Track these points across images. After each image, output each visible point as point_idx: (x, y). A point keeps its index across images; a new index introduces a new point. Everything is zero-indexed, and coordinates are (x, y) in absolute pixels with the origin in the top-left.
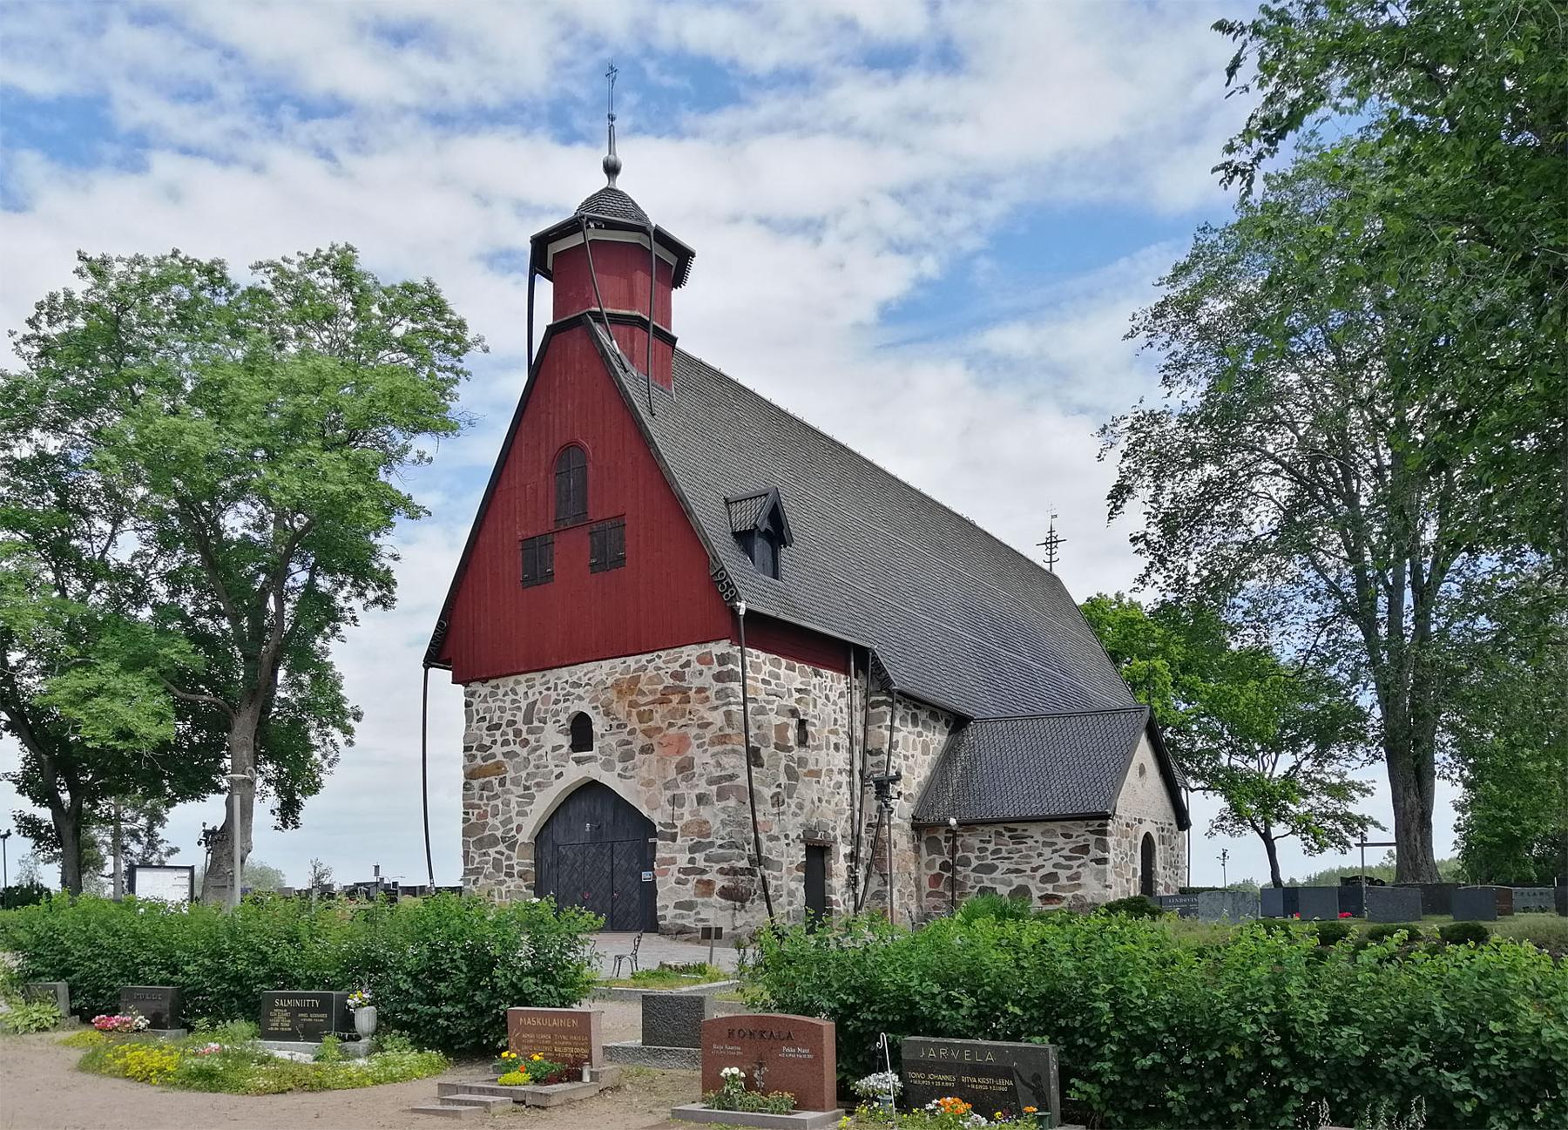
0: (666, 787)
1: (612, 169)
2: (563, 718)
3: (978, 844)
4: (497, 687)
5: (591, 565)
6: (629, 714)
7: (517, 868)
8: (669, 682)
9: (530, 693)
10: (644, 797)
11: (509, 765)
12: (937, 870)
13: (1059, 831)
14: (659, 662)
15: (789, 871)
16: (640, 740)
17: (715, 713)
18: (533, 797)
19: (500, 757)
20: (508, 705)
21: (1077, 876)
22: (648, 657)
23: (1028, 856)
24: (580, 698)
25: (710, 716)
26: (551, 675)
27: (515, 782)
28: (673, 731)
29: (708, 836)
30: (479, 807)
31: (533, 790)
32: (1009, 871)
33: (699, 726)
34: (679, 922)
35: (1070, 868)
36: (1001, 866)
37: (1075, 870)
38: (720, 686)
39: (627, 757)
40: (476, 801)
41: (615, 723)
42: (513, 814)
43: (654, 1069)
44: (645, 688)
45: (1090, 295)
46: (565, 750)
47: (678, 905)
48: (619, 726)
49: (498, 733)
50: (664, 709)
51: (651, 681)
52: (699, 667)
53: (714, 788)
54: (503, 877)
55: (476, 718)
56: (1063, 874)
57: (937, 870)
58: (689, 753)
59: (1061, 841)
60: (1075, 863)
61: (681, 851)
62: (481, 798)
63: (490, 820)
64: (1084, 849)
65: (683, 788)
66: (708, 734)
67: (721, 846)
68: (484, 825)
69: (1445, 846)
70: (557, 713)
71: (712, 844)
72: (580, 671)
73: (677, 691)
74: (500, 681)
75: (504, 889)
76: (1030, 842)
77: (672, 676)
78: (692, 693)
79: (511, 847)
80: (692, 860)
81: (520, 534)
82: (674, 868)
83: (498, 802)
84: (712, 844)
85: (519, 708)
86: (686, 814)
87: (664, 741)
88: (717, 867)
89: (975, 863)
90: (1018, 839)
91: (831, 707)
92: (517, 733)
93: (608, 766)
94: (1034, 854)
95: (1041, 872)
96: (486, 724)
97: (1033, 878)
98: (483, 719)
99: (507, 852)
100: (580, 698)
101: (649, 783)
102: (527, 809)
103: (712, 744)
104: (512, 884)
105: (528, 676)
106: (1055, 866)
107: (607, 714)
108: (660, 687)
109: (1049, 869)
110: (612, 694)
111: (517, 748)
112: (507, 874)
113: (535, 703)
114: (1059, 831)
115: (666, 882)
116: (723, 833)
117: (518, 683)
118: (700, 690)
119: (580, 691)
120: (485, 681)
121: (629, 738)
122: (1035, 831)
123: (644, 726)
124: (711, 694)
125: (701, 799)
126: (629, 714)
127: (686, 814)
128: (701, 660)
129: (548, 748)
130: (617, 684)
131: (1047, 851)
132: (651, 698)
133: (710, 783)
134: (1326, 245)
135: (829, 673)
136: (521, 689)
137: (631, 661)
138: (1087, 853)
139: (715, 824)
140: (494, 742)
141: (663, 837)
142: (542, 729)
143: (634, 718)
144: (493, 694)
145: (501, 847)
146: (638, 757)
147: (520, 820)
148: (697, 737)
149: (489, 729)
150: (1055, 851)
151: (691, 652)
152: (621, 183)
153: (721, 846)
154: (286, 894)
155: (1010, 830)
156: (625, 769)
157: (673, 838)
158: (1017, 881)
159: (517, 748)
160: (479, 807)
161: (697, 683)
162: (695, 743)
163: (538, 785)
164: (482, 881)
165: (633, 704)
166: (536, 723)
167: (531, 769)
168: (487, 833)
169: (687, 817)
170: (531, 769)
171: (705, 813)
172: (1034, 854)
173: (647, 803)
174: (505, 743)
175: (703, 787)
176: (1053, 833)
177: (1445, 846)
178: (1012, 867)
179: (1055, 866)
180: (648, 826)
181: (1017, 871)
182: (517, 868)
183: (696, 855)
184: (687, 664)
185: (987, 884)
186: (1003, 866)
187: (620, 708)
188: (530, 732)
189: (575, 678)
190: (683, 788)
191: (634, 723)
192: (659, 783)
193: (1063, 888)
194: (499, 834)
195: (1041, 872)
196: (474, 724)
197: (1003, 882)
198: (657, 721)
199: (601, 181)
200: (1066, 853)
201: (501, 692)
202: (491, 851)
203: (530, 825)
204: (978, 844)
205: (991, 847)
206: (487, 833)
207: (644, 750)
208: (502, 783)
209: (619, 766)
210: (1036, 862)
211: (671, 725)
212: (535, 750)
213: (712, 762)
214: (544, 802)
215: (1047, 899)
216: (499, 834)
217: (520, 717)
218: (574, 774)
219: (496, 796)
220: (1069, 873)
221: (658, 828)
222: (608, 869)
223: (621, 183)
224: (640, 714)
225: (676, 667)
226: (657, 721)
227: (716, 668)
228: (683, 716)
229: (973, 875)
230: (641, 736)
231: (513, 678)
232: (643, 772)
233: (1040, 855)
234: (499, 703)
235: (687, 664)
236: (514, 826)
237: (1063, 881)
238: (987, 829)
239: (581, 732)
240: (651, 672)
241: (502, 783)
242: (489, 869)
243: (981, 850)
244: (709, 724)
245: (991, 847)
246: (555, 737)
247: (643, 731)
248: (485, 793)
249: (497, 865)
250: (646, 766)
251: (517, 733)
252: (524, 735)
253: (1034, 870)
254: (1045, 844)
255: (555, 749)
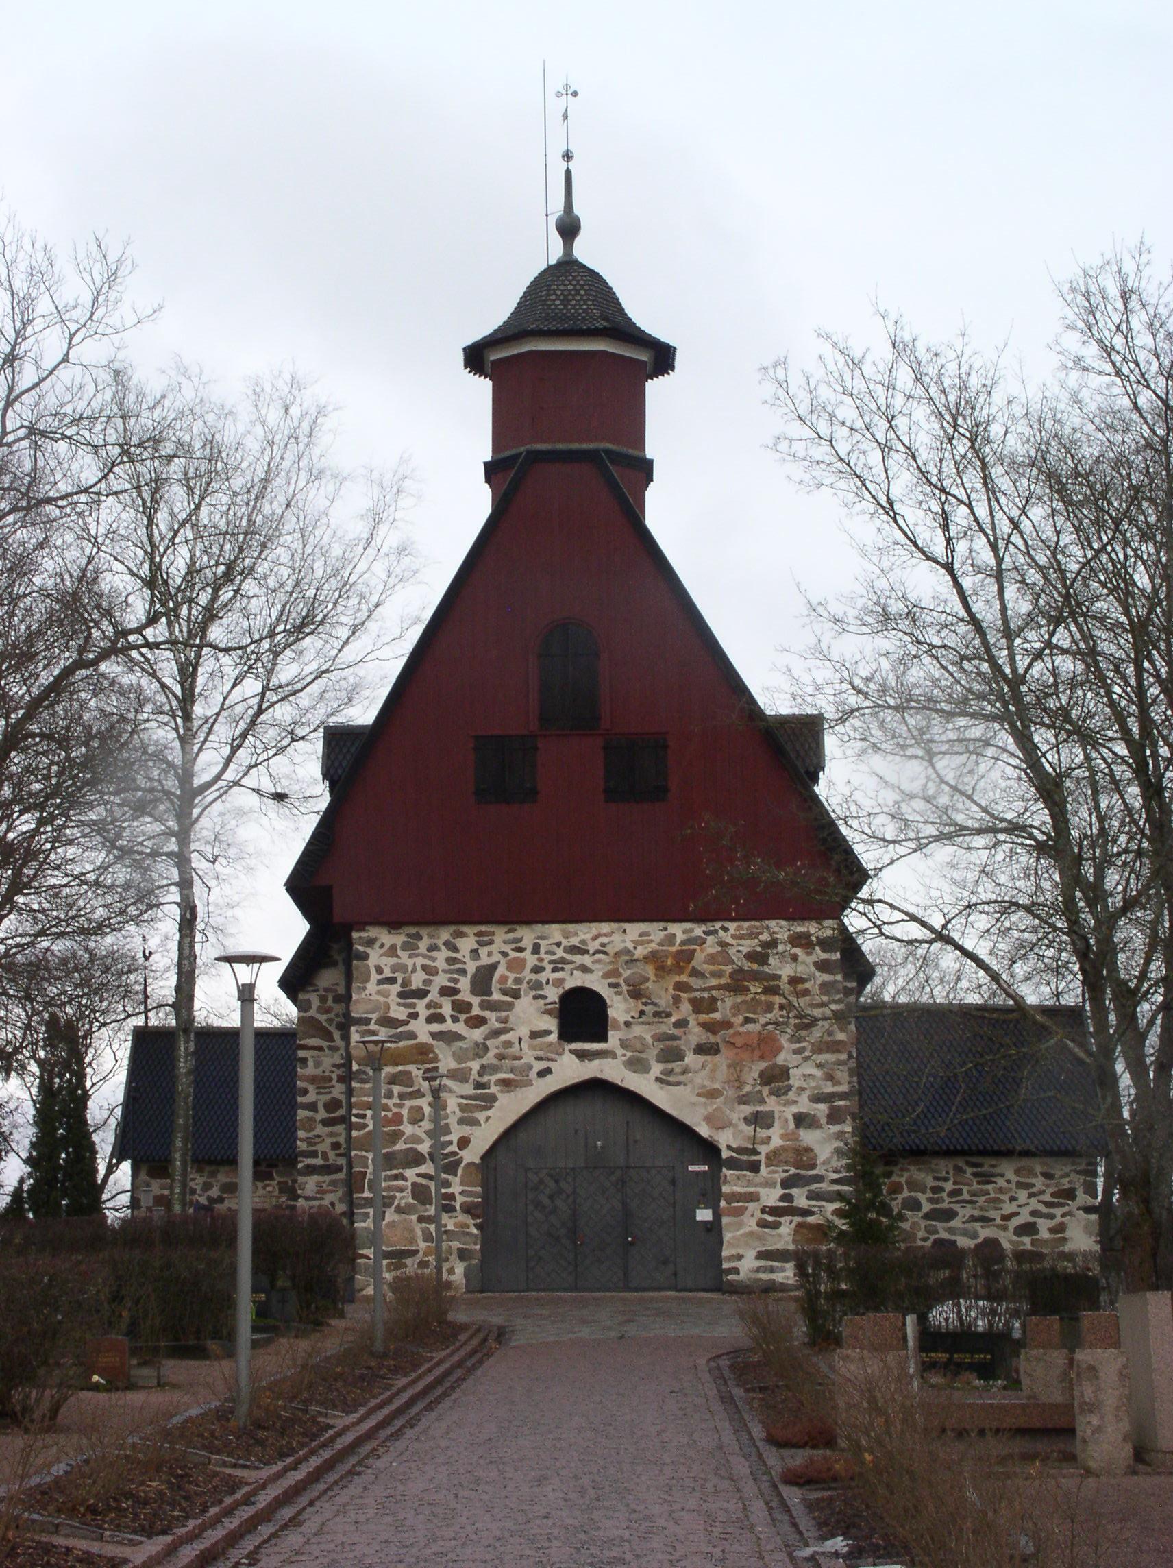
0: (743, 1100)
2: (553, 994)
3: (930, 1183)
4: (419, 937)
6: (677, 1000)
7: (460, 1199)
9: (483, 952)
10: (703, 1112)
18: (493, 1098)
20: (440, 964)
21: (1060, 1228)
24: (585, 969)
29: (813, 1166)
32: (973, 1219)
34: (765, 1276)
35: (1052, 1217)
36: (961, 1212)
37: (1058, 1219)
41: (649, 1009)
47: (762, 1255)
48: (656, 1014)
56: (1044, 1226)
58: (781, 1059)
59: (1039, 1182)
60: (1058, 1212)
61: (769, 1184)
63: (408, 1129)
64: (1070, 1194)
65: (772, 1104)
67: (835, 1182)
72: (584, 933)
76: (1001, 1182)
80: (786, 1198)
85: (463, 972)
86: (776, 1138)
89: (926, 1207)
92: (461, 1007)
94: (1005, 1197)
95: (1015, 1222)
96: (396, 988)
97: (1005, 1228)
98: (392, 981)
100: (585, 969)
102: (481, 1116)
111: (460, 1028)
113: (494, 967)
115: (740, 1225)
119: (587, 960)
121: (676, 1032)
125: (801, 1120)
127: (776, 1138)
129: (524, 1032)
130: (653, 957)
131: (1022, 1195)
132: (714, 982)
138: (1073, 1198)
140: (414, 1016)
141: (732, 1164)
142: (510, 1006)
143: (686, 1007)
144: (406, 946)
145: (427, 1168)
147: (466, 1130)
150: (1031, 1195)
151: (780, 929)
156: (669, 1073)
157: (754, 1167)
159: (460, 1028)
166: (496, 996)
167: (489, 1058)
169: (777, 1142)
170: (489, 1058)
171: (809, 1137)
172: (1005, 1197)
175: (804, 1105)
178: (977, 1213)
180: (709, 1150)
181: (984, 1220)
182: (460, 1199)
183: (794, 1191)
185: (944, 1235)
186: (964, 1212)
189: (574, 941)
190: (772, 1104)
194: (424, 1148)
195: (1015, 1222)
197: (965, 1233)
200: (1047, 1198)
201: (423, 946)
203: (484, 1135)
204: (930, 1183)
205: (949, 1186)
207: (701, 1049)
209: (657, 1069)
210: (1009, 1208)
212: (496, 1033)
218: (570, 1069)
221: (725, 1154)
223: (583, 251)
229: (923, 1223)
233: (1013, 1199)
234: (420, 961)
235: (773, 943)
236: (454, 1137)
237: (1044, 1234)
239: (581, 1017)
240: (711, 946)
242: (405, 1198)
243: (936, 1190)
245: (949, 1186)
246: (532, 1016)
248: (396, 1089)
249: (420, 1194)
251: (461, 1007)
253: (1006, 1218)
254: (1020, 1185)
255: (534, 1035)
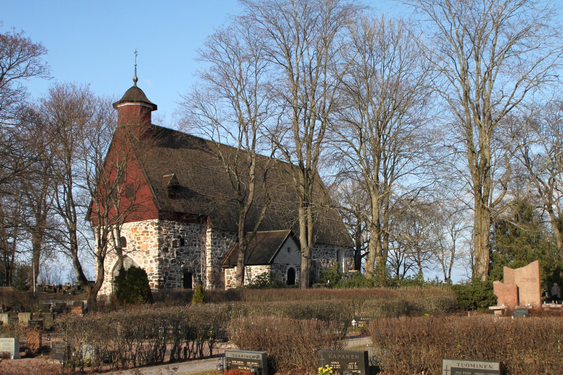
1: (136, 81)
8: (144, 230)
15: (178, 280)
69: (117, 245)
91: (193, 234)
110: (131, 232)
118: (151, 232)
134: (58, 166)
135: (193, 224)
162: (150, 246)
165: (136, 235)
169: (148, 267)
177: (117, 245)
184: (148, 225)
198: (141, 240)
199: (132, 84)
223: (139, 85)
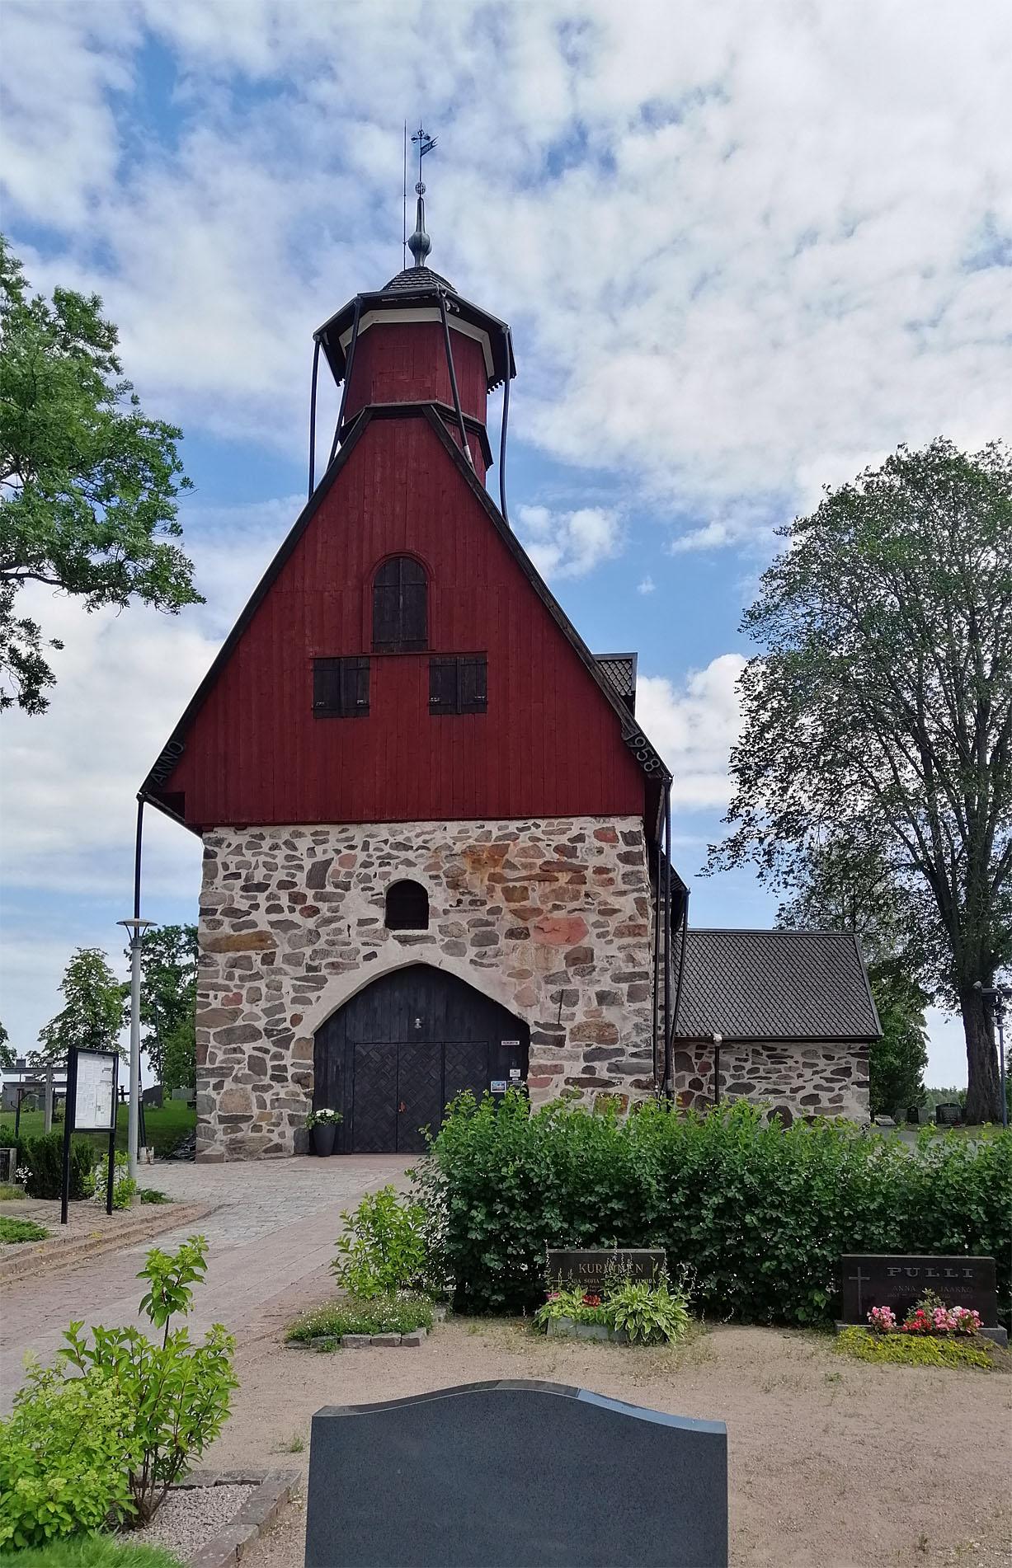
0: (549, 980)
2: (380, 886)
3: (734, 1063)
5: (431, 704)
6: (491, 890)
7: (291, 1071)
9: (319, 849)
10: (512, 990)
11: (278, 936)
12: (686, 1088)
13: (821, 1052)
14: (538, 833)
16: (508, 921)
17: (622, 899)
19: (263, 926)
21: (839, 1098)
22: (520, 824)
23: (786, 1077)
25: (616, 902)
26: (358, 833)
27: (291, 959)
28: (557, 914)
29: (614, 1041)
30: (227, 989)
31: (324, 972)
32: (767, 1091)
33: (601, 913)
35: (832, 1090)
37: (837, 1092)
38: (629, 868)
39: (485, 939)
40: (221, 981)
41: (467, 898)
42: (287, 1000)
43: (448, 1326)
44: (516, 861)
45: (241, 527)
46: (380, 925)
48: (473, 903)
49: (261, 898)
50: (548, 887)
51: (524, 852)
52: (598, 844)
53: (625, 986)
54: (267, 1080)
55: (221, 873)
56: (825, 1096)
57: (686, 1088)
58: (585, 942)
59: (822, 1063)
60: (837, 1085)
62: (230, 977)
63: (245, 1006)
65: (576, 983)
66: (613, 923)
67: (634, 1055)
68: (236, 1014)
70: (367, 879)
71: (621, 1052)
72: (409, 831)
73: (563, 864)
74: (266, 831)
75: (268, 1097)
76: (790, 1063)
77: (557, 849)
78: (589, 873)
79: (284, 1042)
81: (311, 651)
82: (559, 1079)
83: (261, 984)
84: (621, 1052)
85: (300, 867)
86: (579, 1015)
87: (546, 926)
88: (630, 1079)
89: (730, 1082)
90: (778, 1059)
93: (454, 948)
97: (793, 1099)
98: (237, 876)
99: (273, 1049)
100: (409, 863)
101: (522, 974)
102: (312, 996)
103: (619, 933)
104: (281, 1091)
105: (319, 828)
106: (815, 1087)
107: (454, 885)
108: (540, 862)
109: (809, 1090)
110: (465, 864)
111: (296, 917)
112: (273, 1077)
113: (328, 862)
114: (821, 1052)
116: (638, 1040)
117: (300, 835)
118: (600, 871)
119: (410, 855)
120: (240, 827)
121: (491, 918)
122: (796, 1051)
123: (515, 905)
124: (617, 876)
125: (603, 997)
126: (491, 890)
127: (579, 1015)
128: (600, 835)
129: (352, 920)
131: (808, 1072)
132: (524, 873)
133: (618, 979)
136: (303, 844)
137: (492, 826)
138: (849, 1075)
139: (625, 1028)
141: (541, 1039)
142: (342, 897)
143: (499, 893)
144: (250, 846)
145: (264, 1042)
146: (503, 942)
147: (298, 1009)
148: (596, 925)
149: (245, 888)
150: (816, 1072)
151: (586, 825)
152: (429, 262)
153: (634, 1055)
154: (961, 1095)
155: (768, 1049)
157: (560, 1042)
158: (774, 1101)
159: (296, 917)
160: (227, 989)
161: (594, 861)
163: (333, 965)
164: (228, 1084)
165: (494, 878)
166: (329, 888)
167: (321, 944)
168: (239, 1022)
169: (580, 1018)
170: (321, 944)
171: (609, 1014)
173: (517, 997)
174: (276, 909)
175: (606, 984)
176: (815, 1054)
178: (770, 1087)
179: (815, 1087)
181: (775, 1091)
182: (291, 1071)
183: (596, 1064)
186: (761, 1086)
187: (478, 883)
188: (320, 897)
189: (400, 839)
190: (576, 983)
191: (498, 900)
192: (538, 975)
193: (825, 1110)
194: (261, 1025)
196: (219, 881)
200: (827, 1074)
201: (266, 845)
202: (248, 1048)
203: (315, 1015)
204: (734, 1063)
205: (748, 1065)
206: (239, 1022)
207: (512, 934)
208: (268, 960)
209: (472, 952)
211: (556, 907)
213: (621, 955)
214: (340, 989)
215: (809, 1120)
216: (261, 1025)
217: (301, 878)
218: (394, 954)
219: (257, 976)
220: (831, 1095)
221: (533, 1030)
222: (436, 1075)
223: (429, 262)
224: (506, 891)
225: (563, 840)
226: (534, 899)
227: (622, 847)
228: (576, 897)
230: (509, 916)
231: (292, 828)
232: (514, 960)
233: (800, 1076)
235: (580, 838)
236: (288, 1015)
237: (825, 1103)
238: (743, 1047)
239: (406, 906)
240: (524, 840)
241: (268, 960)
242: (242, 1069)
244: (615, 911)
245: (748, 1065)
246: (362, 907)
247: (514, 912)
248: (237, 972)
249: (256, 1065)
250: (522, 954)
252: (310, 902)
253: (794, 1091)
254: (805, 1065)
255: (362, 923)
